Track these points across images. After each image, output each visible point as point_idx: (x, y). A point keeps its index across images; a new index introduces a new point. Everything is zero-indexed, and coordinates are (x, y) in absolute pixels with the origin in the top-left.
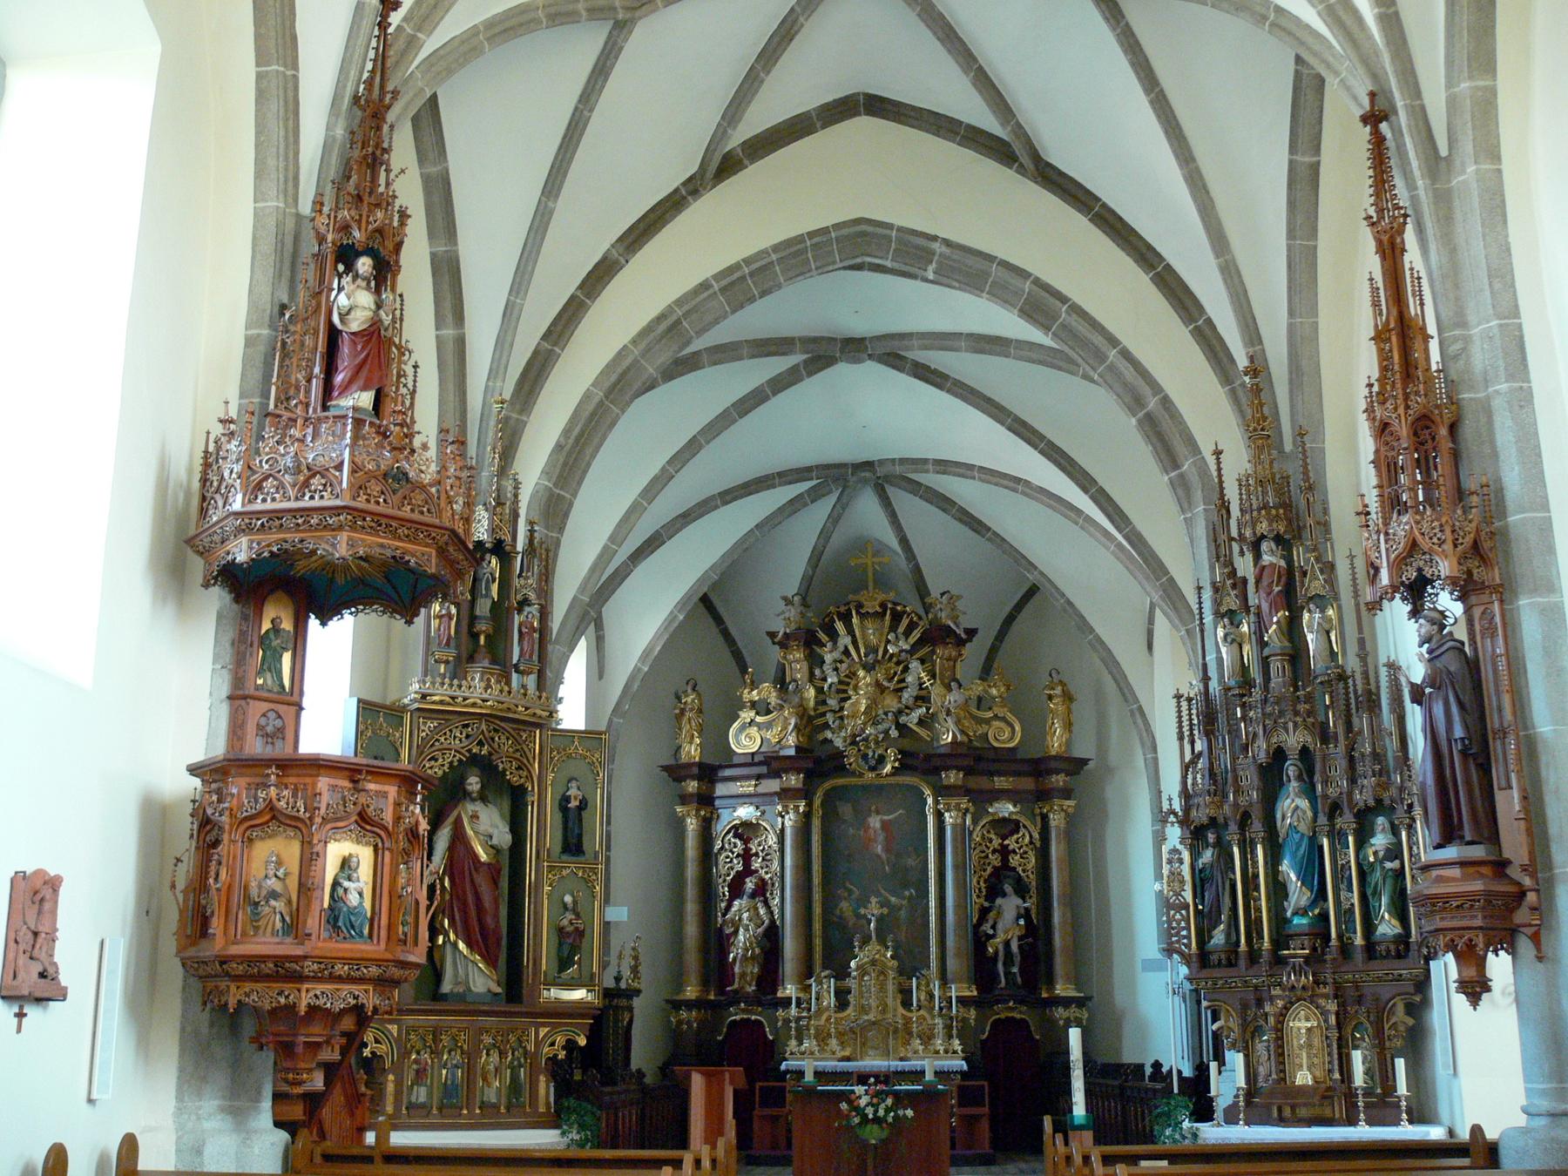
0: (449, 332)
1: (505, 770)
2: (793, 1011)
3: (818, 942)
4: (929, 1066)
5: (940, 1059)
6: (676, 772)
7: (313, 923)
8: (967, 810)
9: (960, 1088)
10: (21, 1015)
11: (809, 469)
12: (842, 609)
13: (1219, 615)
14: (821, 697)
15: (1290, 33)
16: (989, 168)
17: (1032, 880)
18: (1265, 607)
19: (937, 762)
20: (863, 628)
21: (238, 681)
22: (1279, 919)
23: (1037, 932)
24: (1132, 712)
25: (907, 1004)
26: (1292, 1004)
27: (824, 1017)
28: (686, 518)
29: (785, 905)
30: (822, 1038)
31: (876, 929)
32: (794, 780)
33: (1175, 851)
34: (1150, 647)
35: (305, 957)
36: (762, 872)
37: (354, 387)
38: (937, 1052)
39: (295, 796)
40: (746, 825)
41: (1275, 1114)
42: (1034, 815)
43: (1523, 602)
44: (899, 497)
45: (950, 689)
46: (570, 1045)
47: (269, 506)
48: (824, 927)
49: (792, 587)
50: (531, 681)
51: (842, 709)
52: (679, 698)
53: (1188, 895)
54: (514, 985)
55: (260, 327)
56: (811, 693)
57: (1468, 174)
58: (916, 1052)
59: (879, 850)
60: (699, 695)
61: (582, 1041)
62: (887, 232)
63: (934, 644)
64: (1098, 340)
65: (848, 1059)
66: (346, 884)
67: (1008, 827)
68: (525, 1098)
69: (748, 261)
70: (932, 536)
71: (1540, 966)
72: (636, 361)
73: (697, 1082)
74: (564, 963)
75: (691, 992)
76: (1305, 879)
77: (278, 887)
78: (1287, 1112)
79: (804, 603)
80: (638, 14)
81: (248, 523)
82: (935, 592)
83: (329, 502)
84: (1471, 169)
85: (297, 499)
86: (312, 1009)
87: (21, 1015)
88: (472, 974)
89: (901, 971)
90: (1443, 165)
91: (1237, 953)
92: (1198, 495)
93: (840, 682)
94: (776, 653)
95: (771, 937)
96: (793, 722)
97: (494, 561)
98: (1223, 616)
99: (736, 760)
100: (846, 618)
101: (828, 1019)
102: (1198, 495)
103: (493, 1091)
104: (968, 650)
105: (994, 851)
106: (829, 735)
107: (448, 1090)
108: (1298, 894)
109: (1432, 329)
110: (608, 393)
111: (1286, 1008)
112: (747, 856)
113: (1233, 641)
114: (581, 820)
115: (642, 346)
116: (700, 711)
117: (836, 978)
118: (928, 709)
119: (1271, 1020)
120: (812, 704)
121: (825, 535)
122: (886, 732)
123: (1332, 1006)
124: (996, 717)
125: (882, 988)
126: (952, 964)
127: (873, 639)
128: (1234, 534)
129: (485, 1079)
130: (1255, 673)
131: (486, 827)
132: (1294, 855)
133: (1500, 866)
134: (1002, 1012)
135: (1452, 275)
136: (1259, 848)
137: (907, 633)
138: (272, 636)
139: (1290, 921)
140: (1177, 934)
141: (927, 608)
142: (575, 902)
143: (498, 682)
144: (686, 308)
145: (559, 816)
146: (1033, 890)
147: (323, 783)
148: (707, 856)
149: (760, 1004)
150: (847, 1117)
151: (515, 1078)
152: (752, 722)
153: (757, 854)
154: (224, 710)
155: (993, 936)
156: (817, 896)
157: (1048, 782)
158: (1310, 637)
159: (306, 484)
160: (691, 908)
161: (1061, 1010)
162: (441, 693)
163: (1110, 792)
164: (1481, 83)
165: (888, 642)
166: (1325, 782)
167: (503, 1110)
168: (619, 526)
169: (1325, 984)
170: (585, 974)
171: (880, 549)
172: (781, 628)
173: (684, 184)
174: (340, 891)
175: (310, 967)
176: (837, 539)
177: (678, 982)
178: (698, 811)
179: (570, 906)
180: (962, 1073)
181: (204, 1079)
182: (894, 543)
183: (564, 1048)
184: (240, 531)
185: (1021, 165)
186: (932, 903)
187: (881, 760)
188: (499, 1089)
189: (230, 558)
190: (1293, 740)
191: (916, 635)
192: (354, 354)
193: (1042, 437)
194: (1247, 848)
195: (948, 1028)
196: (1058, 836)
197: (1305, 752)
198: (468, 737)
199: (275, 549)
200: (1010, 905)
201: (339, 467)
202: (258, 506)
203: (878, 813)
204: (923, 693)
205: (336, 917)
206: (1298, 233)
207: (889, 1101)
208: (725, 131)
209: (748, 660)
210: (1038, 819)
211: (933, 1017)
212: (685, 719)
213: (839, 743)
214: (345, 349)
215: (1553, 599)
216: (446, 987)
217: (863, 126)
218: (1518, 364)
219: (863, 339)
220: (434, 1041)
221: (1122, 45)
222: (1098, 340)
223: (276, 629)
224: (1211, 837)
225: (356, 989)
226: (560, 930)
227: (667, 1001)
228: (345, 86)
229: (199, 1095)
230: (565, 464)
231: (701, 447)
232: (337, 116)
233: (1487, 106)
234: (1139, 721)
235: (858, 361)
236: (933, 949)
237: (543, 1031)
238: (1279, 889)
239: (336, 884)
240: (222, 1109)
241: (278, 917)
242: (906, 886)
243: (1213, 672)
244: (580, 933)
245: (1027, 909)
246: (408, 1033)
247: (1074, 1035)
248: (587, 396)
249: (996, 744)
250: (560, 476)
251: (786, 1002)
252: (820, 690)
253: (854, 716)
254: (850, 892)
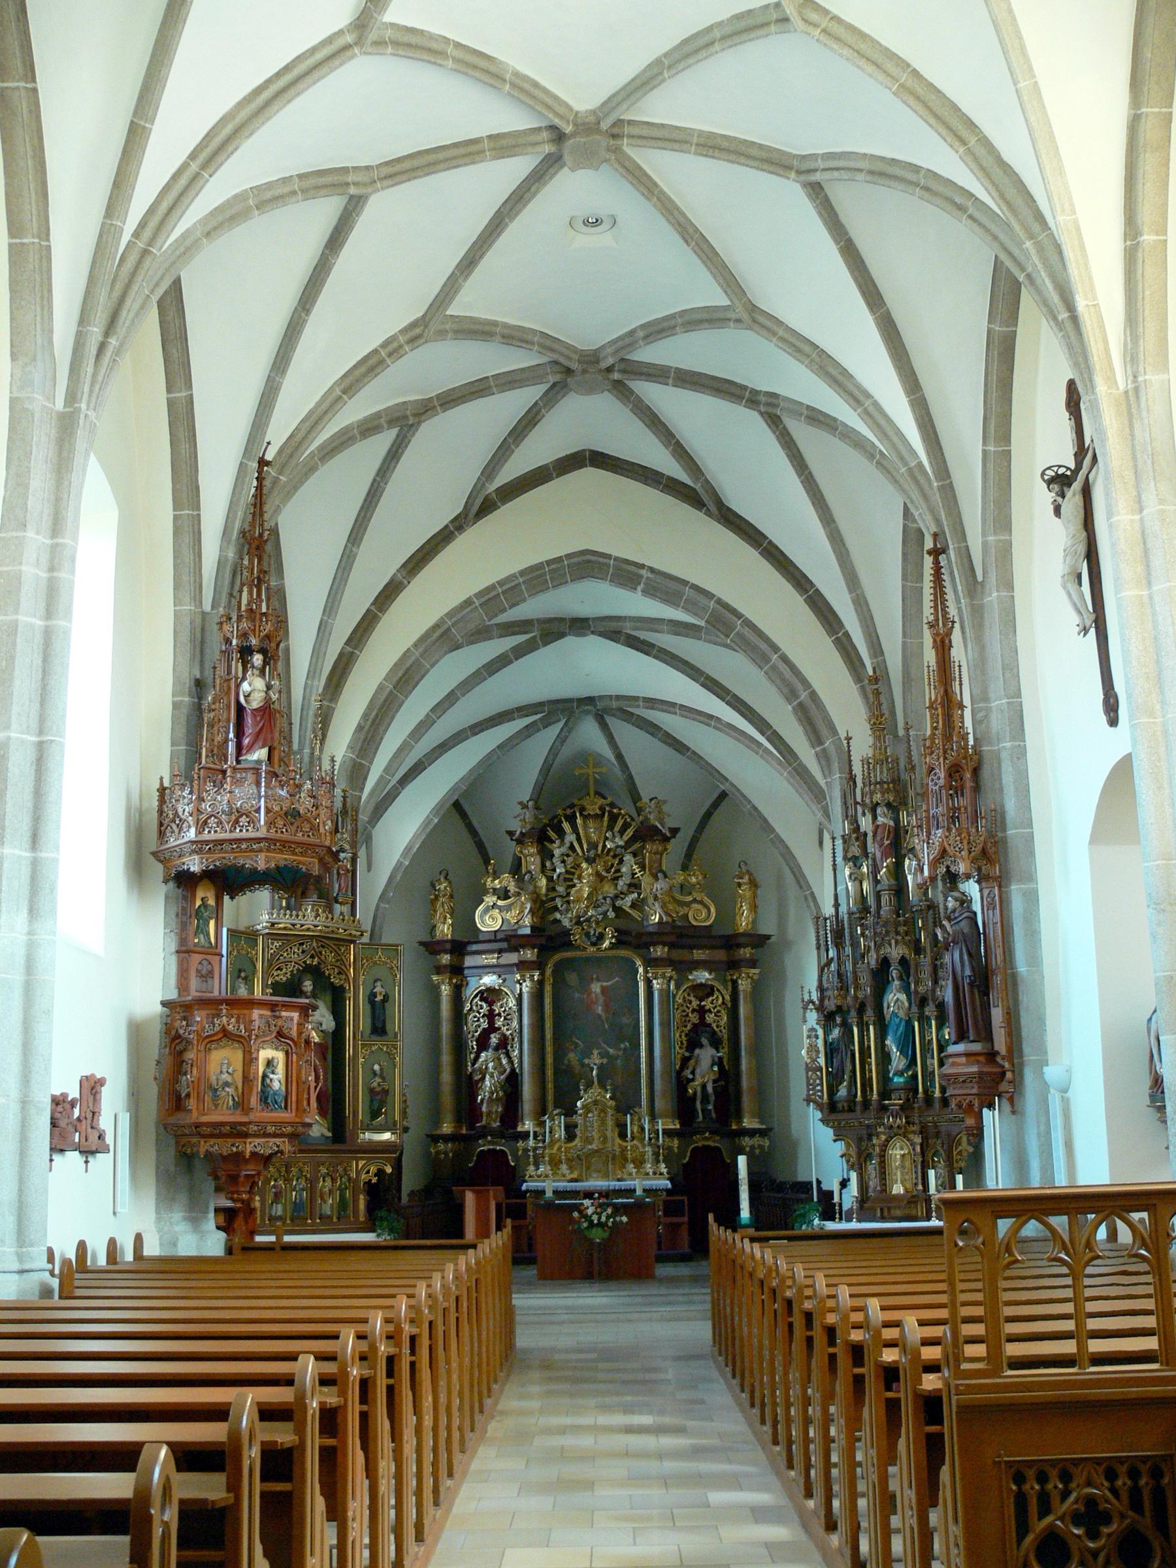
2: (531, 1142)
3: (550, 1086)
4: (638, 1185)
5: (650, 1179)
6: (432, 947)
7: (254, 1101)
8: (671, 978)
9: (665, 1202)
10: (87, 1162)
11: (541, 704)
12: (569, 812)
13: (846, 859)
14: (551, 884)
15: (889, 472)
16: (685, 510)
17: (724, 1034)
18: (878, 855)
19: (645, 939)
20: (585, 827)
21: (183, 941)
22: (884, 1078)
23: (728, 1076)
24: (806, 899)
25: (623, 1135)
27: (556, 1147)
28: (443, 748)
29: (523, 1056)
30: (555, 1163)
31: (598, 1075)
32: (529, 954)
33: (813, 1029)
35: (250, 1123)
36: (504, 1029)
37: (256, 746)
38: (648, 1174)
39: (238, 1021)
40: (490, 990)
41: (879, 1214)
42: (726, 981)
43: (1013, 887)
44: (614, 723)
45: (657, 879)
46: (380, 1173)
47: (213, 836)
48: (555, 1074)
49: (525, 794)
50: (346, 909)
51: (568, 894)
52: (433, 886)
53: (822, 1061)
54: (339, 1131)
55: (183, 695)
56: (543, 882)
57: (993, 597)
58: (631, 1174)
59: (600, 1010)
60: (450, 883)
61: (389, 1170)
62: (605, 561)
63: (644, 841)
64: (764, 646)
65: (576, 1180)
66: (272, 1076)
67: (704, 991)
68: (350, 1211)
69: (501, 583)
70: (639, 749)
71: (1014, 1117)
72: (417, 660)
73: (470, 1198)
74: (375, 1114)
75: (447, 1128)
77: (229, 1079)
78: (886, 1213)
79: (537, 808)
81: (199, 847)
82: (645, 799)
83: (252, 834)
84: (995, 594)
85: (231, 831)
86: (254, 1154)
87: (87, 1162)
89: (618, 1109)
90: (979, 587)
91: (855, 1102)
92: (835, 766)
93: (567, 872)
94: (512, 847)
95: (513, 1081)
96: (529, 906)
98: (849, 860)
99: (481, 938)
100: (571, 819)
101: (559, 1149)
102: (835, 766)
103: (328, 1206)
104: (671, 846)
105: (694, 1011)
106: (558, 916)
107: (297, 1206)
108: (898, 1060)
109: (967, 701)
111: (887, 1141)
112: (491, 1016)
113: (856, 879)
116: (451, 896)
117: (566, 1115)
118: (639, 894)
119: (877, 1149)
120: (544, 891)
121: (554, 751)
122: (605, 914)
123: (918, 1140)
124: (695, 901)
125: (603, 1122)
126: (659, 1104)
127: (594, 837)
128: (859, 799)
130: (871, 901)
133: (991, 1056)
134: (699, 1141)
135: (981, 665)
136: (871, 1028)
137: (622, 832)
139: (892, 1080)
140: (814, 1089)
141: (639, 811)
142: (381, 1069)
143: (324, 911)
145: (368, 1007)
146: (725, 1042)
147: (256, 1013)
148: (459, 1017)
149: (503, 1137)
150: (579, 1222)
151: (342, 1196)
152: (494, 906)
153: (499, 1014)
154: (173, 960)
155: (693, 1080)
156: (549, 1049)
157: (739, 952)
158: (909, 878)
159: (237, 822)
160: (446, 1059)
161: (747, 1139)
162: (285, 921)
163: (789, 961)
164: (1002, 538)
165: (606, 838)
166: (917, 984)
169: (913, 1124)
170: (390, 1122)
171: (598, 760)
172: (517, 827)
173: (452, 522)
174: (268, 1081)
176: (566, 752)
177: (437, 1122)
178: (451, 979)
180: (667, 1190)
181: (173, 1199)
182: (609, 754)
184: (194, 852)
185: (708, 509)
186: (643, 1054)
187: (601, 937)
188: (332, 1205)
189: (186, 867)
190: (895, 952)
191: (629, 833)
192: (256, 723)
193: (728, 692)
195: (656, 1154)
196: (745, 998)
197: (903, 961)
198: (303, 952)
199: (218, 864)
200: (706, 1055)
201: (258, 810)
202: (206, 836)
203: (598, 980)
204: (636, 881)
205: (264, 1098)
206: (909, 578)
207: (609, 1211)
209: (491, 855)
210: (730, 984)
211: (644, 1146)
212: (439, 904)
213: (566, 923)
214: (249, 720)
215: (1032, 886)
217: (589, 474)
218: (1019, 731)
219: (587, 619)
221: (780, 443)
222: (764, 646)
223: (204, 904)
224: (838, 1020)
225: (278, 1141)
226: (372, 1091)
227: (428, 1136)
228: (234, 522)
229: (171, 1211)
230: (365, 740)
232: (229, 542)
233: (1005, 552)
234: (812, 904)
235: (584, 635)
236: (644, 1091)
237: (361, 1163)
238: (885, 1057)
239: (265, 1076)
240: (185, 1219)
242: (621, 1039)
243: (842, 900)
245: (720, 1058)
247: (742, 1161)
248: (381, 688)
249: (695, 923)
250: (360, 750)
251: (525, 1136)
252: (550, 879)
253: (578, 901)
254: (577, 1045)
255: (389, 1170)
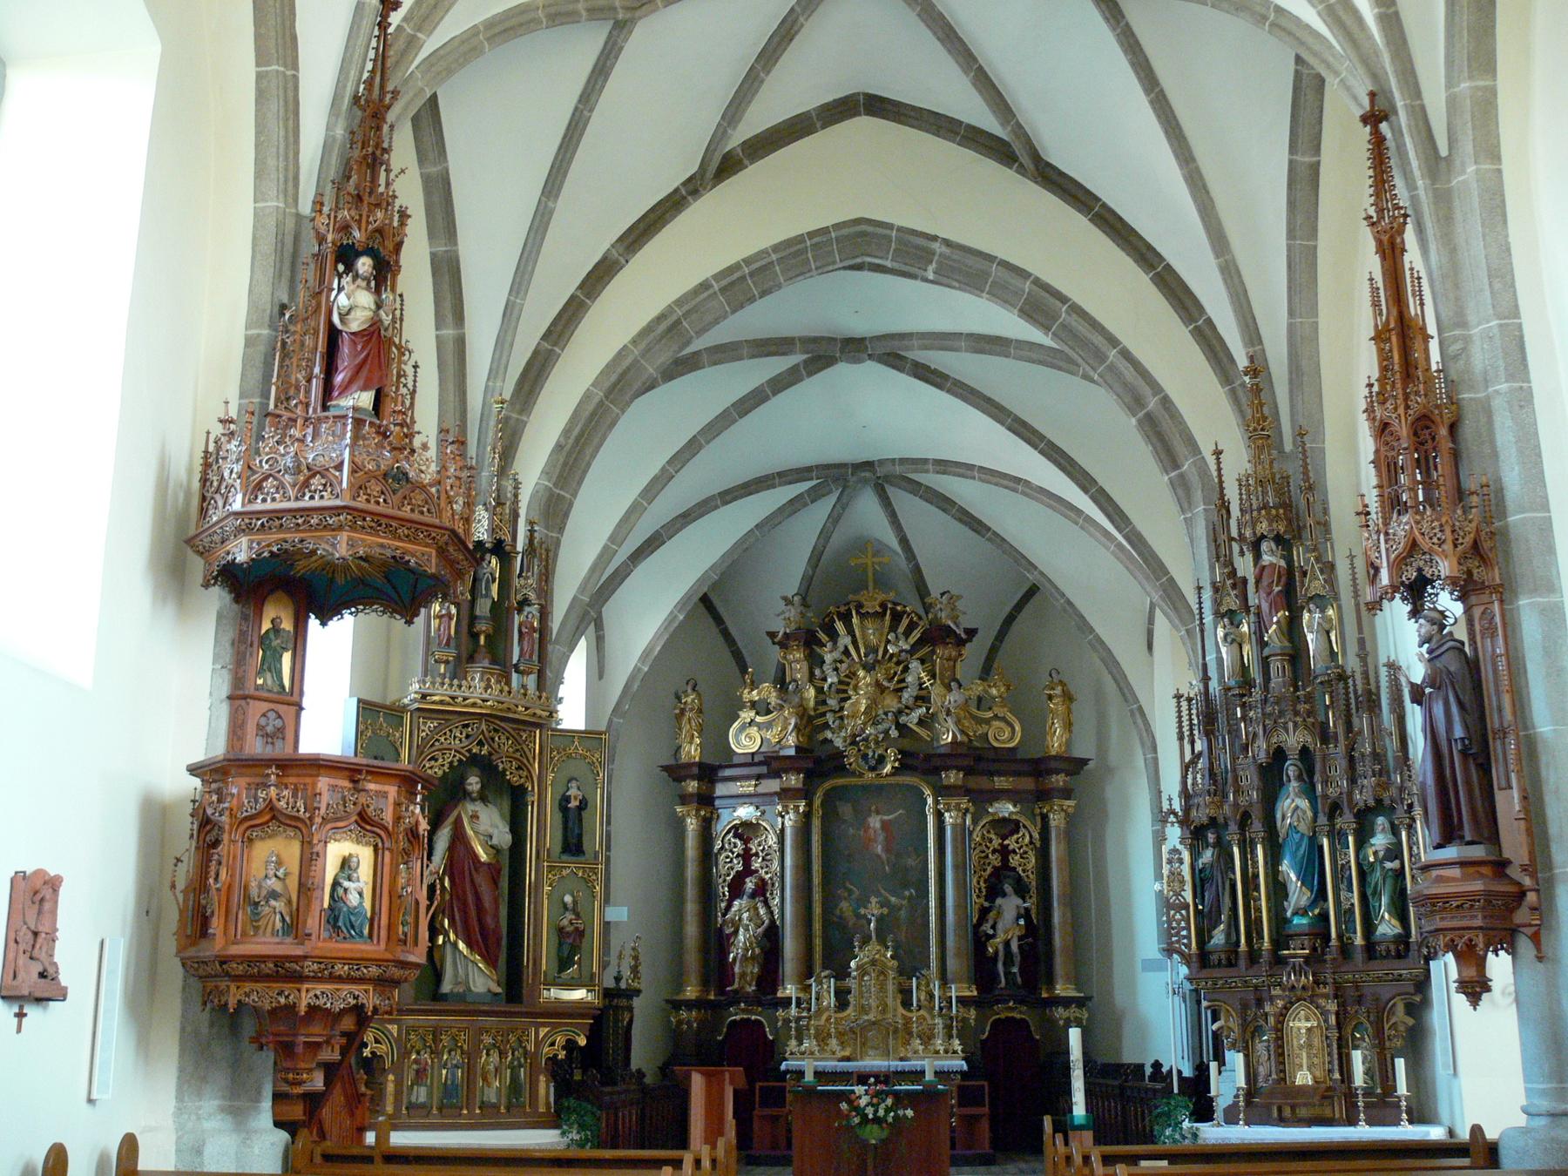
0: (449, 332)
1: (505, 770)
2: (793, 1011)
3: (818, 942)
4: (929, 1066)
5: (940, 1059)
6: (676, 772)
7: (313, 923)
8: (967, 810)
9: (960, 1088)
10: (21, 1015)
11: (809, 469)
12: (842, 609)
13: (1219, 615)
14: (821, 697)
15: (1290, 33)
16: (989, 168)
17: (1032, 880)
18: (1265, 607)
19: (937, 762)
20: (863, 628)
21: (238, 681)
22: (1279, 919)
23: (1037, 932)
24: (1132, 712)
25: (907, 1004)
26: (1292, 1004)
27: (824, 1017)
28: (686, 518)
29: (785, 905)
30: (822, 1038)
31: (876, 929)
32: (794, 780)
33: (1175, 851)
34: (1150, 647)
35: (305, 957)
36: (762, 872)
37: (354, 387)
38: (937, 1052)
39: (295, 796)
40: (746, 825)
41: (1275, 1114)
42: (1034, 815)
43: (1523, 602)
44: (899, 497)
45: (950, 689)
46: (570, 1045)
47: (269, 506)
48: (824, 927)
49: (792, 587)
50: (531, 681)
51: (842, 709)
52: (679, 698)
53: (1188, 895)
54: (514, 985)
55: (260, 327)
56: (811, 693)
57: (1468, 174)
58: (916, 1052)
59: (879, 850)
60: (699, 695)
61: (582, 1041)
62: (887, 232)
63: (934, 644)
64: (1098, 340)
65: (848, 1059)
66: (346, 884)
67: (1008, 827)
68: (525, 1098)
69: (748, 261)
70: (932, 536)
71: (1540, 966)
72: (636, 361)
73: (697, 1082)
74: (564, 963)
75: (691, 992)
76: (1305, 879)
77: (278, 887)
78: (1287, 1112)
79: (804, 603)
80: (638, 14)
81: (248, 523)
82: (935, 592)
83: (329, 502)
84: (1471, 169)
85: (297, 499)
86: (312, 1009)
87: (21, 1015)
88: (472, 974)
89: (901, 971)
90: (1443, 165)
91: (1237, 953)
92: (1198, 495)
93: (840, 682)
94: (776, 653)
95: (771, 937)
96: (793, 722)
97: (494, 561)
98: (1223, 616)
99: (736, 760)
100: (846, 618)
101: (828, 1019)
102: (1198, 495)
103: (493, 1091)
104: (968, 650)
105: (994, 851)
106: (829, 735)
107: (448, 1090)
108: (1298, 894)
109: (1432, 329)
110: (608, 393)
111: (1286, 1008)
112: (747, 856)
113: (1233, 641)
114: (581, 820)
115: (642, 346)
116: (700, 711)
117: (836, 978)
118: (928, 709)
119: (1271, 1020)
120: (812, 704)
121: (825, 535)
122: (886, 732)
123: (1332, 1006)
124: (996, 717)
125: (882, 988)
126: (952, 964)
127: (873, 639)
128: (1234, 534)
129: (485, 1079)
130: (1255, 673)
131: (486, 827)
132: (1294, 855)
133: (1500, 866)
134: (1002, 1012)
135: (1452, 275)
136: (1259, 848)
137: (907, 633)
138: (272, 636)
139: (1290, 921)
140: (1177, 934)
141: (927, 608)
142: (575, 902)
143: (498, 682)
144: (686, 308)
145: (559, 816)
146: (1033, 890)
147: (323, 783)
148: (707, 856)
149: (760, 1004)
150: (847, 1117)
151: (515, 1078)
152: (752, 722)
153: (757, 854)
154: (224, 710)
155: (993, 936)
156: (817, 896)
157: (1048, 782)
158: (1310, 637)
159: (306, 484)
160: (691, 908)
161: (1061, 1010)
162: (441, 693)
163: (1110, 792)
164: (1481, 83)
165: (888, 642)
166: (1325, 782)
167: (503, 1110)
168: (619, 526)
169: (1325, 984)
170: (585, 974)
171: (880, 549)
172: (781, 628)
173: (684, 184)
174: (340, 891)
175: (310, 967)
176: (837, 539)
177: (678, 982)
178: (698, 811)
179: (570, 906)
180: (962, 1073)
181: (204, 1079)
182: (894, 543)
183: (564, 1048)
184: (240, 531)
185: (1021, 165)
186: (932, 903)
187: (881, 760)
188: (499, 1089)
189: (230, 558)
190: (1293, 740)
191: (916, 635)
192: (354, 354)
193: (1042, 437)
194: (1247, 848)
195: (948, 1028)
196: (1058, 836)
197: (1305, 752)
198: (468, 737)
199: (275, 549)
200: (1010, 905)
201: (339, 467)
202: (258, 506)
203: (878, 813)
204: (923, 693)
205: (336, 917)
206: (1298, 233)
207: (889, 1101)
208: (725, 131)
209: (748, 660)
210: (1038, 819)
211: (933, 1017)
212: (685, 719)
213: (839, 743)
214: (345, 349)
215: (1553, 599)
216: (446, 987)
217: (863, 126)
218: (1518, 364)
219: (863, 339)
220: (434, 1041)
221: (1122, 45)
222: (1098, 340)
223: (276, 629)
224: (1211, 837)
225: (356, 989)
226: (560, 930)
227: (667, 1001)
228: (345, 86)
229: (199, 1095)
230: (565, 464)
231: (701, 447)
232: (337, 116)
233: (1487, 106)
234: (1139, 721)
235: (858, 361)
236: (933, 949)
237: (543, 1031)
238: (1279, 889)
239: (336, 884)
240: (222, 1109)
241: (278, 917)
242: (906, 886)
244: (580, 933)
245: (1027, 909)
246: (408, 1033)
247: (1074, 1035)
248: (587, 396)
249: (996, 744)
250: (560, 476)
251: (786, 1002)
252: (820, 690)
253: (854, 716)
254: (850, 892)
255: (582, 1041)
